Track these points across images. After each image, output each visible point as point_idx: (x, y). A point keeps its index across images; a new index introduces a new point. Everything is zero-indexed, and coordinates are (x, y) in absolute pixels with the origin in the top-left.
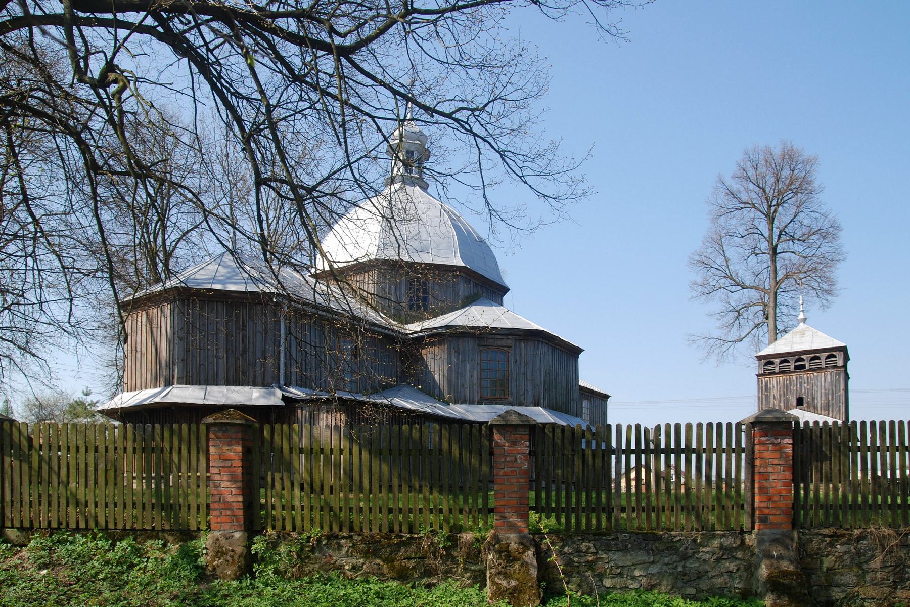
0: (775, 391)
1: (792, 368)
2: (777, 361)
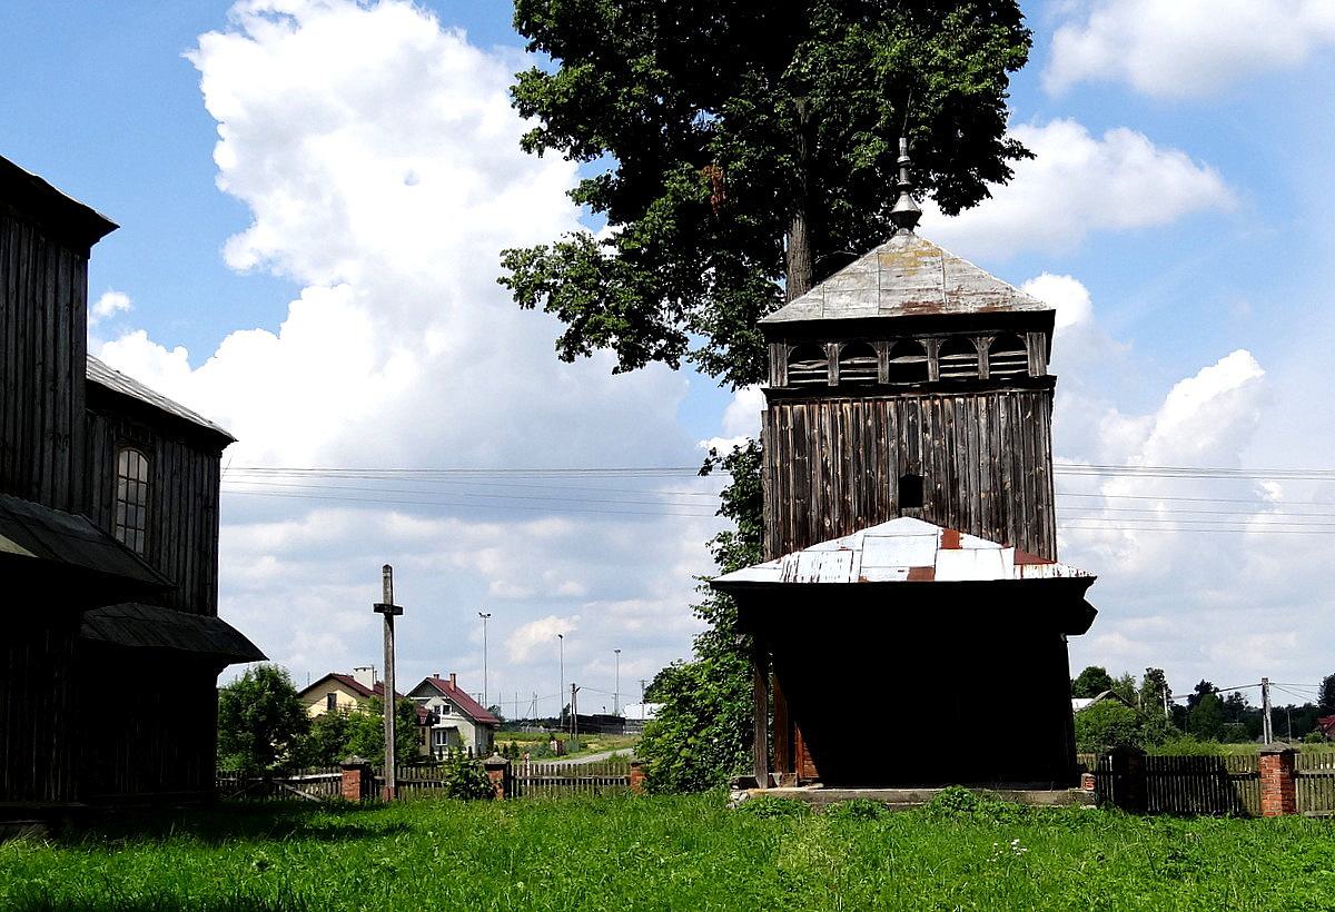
1: (883, 371)
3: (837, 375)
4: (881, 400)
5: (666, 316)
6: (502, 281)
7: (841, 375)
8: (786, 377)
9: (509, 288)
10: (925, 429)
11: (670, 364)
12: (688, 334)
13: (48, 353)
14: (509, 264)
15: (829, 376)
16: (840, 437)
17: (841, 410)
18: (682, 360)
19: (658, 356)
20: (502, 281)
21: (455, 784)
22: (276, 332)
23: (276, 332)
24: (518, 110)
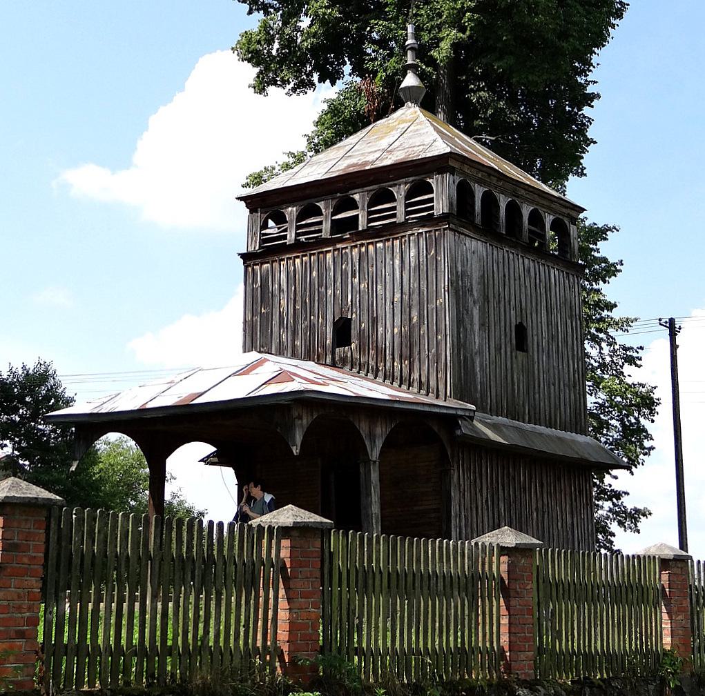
0: (284, 302)
1: (326, 227)
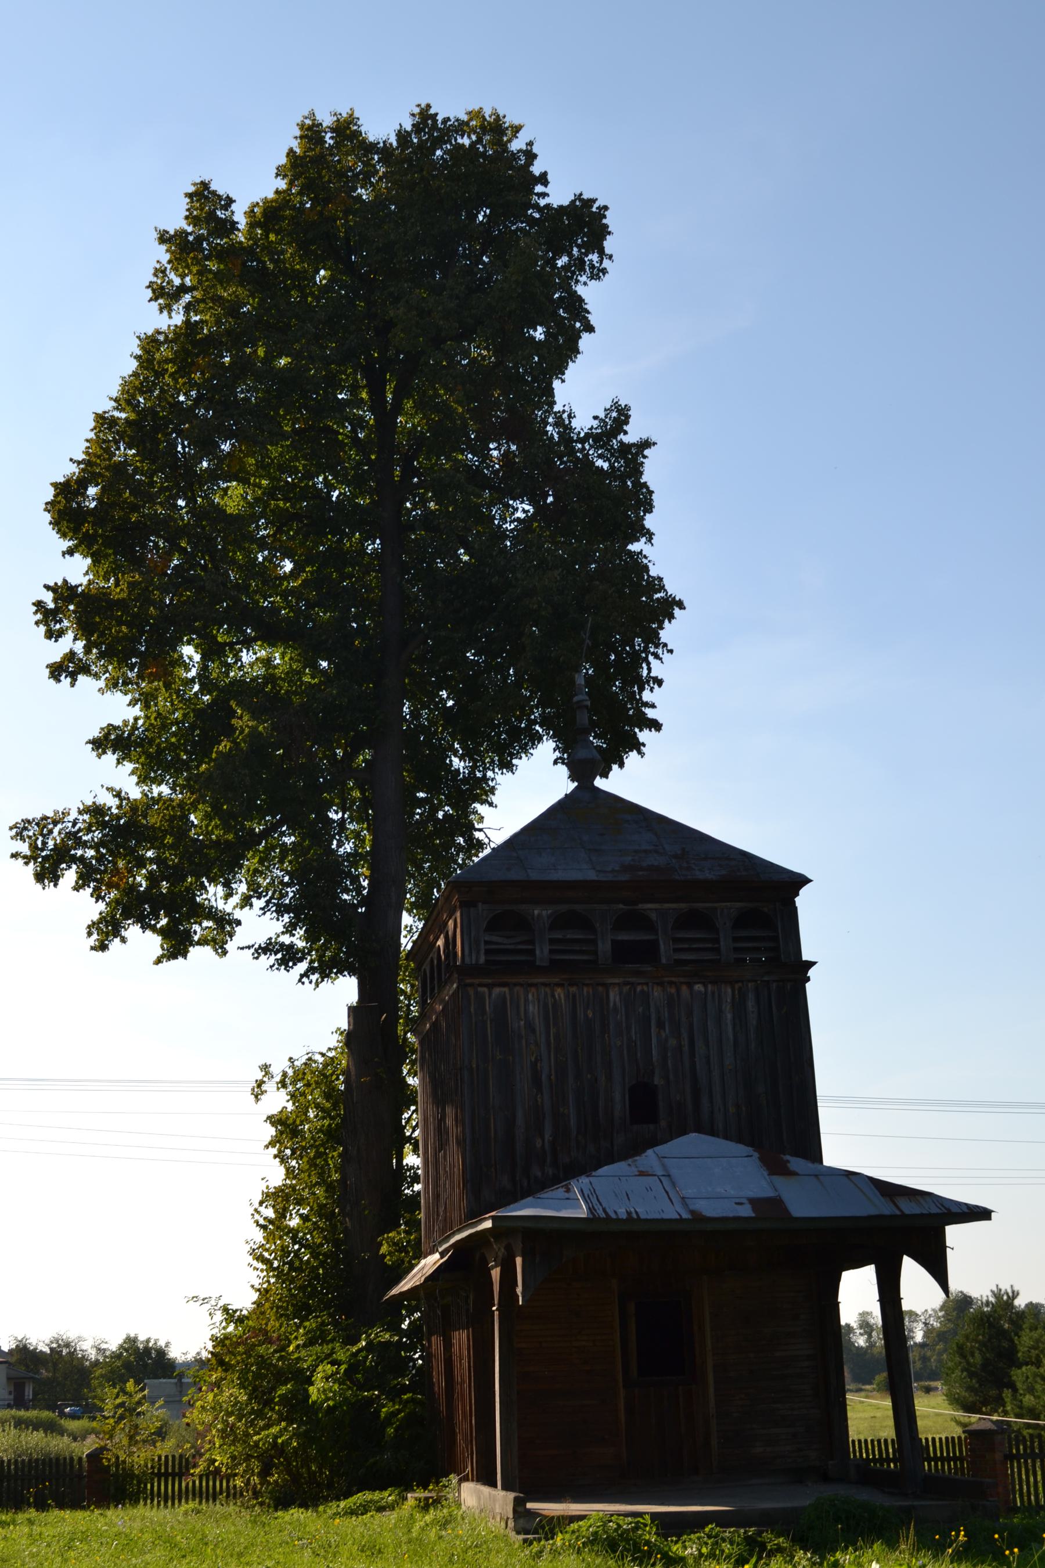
1: (604, 947)
2: (541, 913)
3: (546, 951)
4: (604, 985)
5: (214, 894)
6: (15, 856)
7: (551, 951)
8: (482, 952)
9: (26, 864)
10: (660, 1025)
11: (216, 950)
12: (238, 914)
13: (442, 1367)
14: (20, 836)
15: (538, 952)
16: (552, 1031)
17: (553, 996)
18: (230, 946)
19: (203, 942)
20: (15, 856)
21: (206, 1537)
22: (609, 233)
23: (609, 233)
24: (42, 629)
